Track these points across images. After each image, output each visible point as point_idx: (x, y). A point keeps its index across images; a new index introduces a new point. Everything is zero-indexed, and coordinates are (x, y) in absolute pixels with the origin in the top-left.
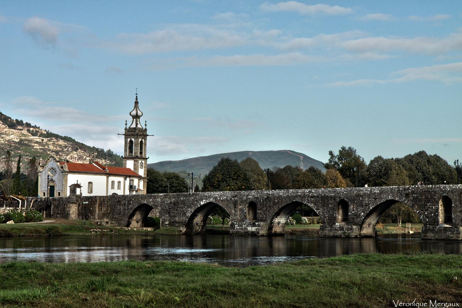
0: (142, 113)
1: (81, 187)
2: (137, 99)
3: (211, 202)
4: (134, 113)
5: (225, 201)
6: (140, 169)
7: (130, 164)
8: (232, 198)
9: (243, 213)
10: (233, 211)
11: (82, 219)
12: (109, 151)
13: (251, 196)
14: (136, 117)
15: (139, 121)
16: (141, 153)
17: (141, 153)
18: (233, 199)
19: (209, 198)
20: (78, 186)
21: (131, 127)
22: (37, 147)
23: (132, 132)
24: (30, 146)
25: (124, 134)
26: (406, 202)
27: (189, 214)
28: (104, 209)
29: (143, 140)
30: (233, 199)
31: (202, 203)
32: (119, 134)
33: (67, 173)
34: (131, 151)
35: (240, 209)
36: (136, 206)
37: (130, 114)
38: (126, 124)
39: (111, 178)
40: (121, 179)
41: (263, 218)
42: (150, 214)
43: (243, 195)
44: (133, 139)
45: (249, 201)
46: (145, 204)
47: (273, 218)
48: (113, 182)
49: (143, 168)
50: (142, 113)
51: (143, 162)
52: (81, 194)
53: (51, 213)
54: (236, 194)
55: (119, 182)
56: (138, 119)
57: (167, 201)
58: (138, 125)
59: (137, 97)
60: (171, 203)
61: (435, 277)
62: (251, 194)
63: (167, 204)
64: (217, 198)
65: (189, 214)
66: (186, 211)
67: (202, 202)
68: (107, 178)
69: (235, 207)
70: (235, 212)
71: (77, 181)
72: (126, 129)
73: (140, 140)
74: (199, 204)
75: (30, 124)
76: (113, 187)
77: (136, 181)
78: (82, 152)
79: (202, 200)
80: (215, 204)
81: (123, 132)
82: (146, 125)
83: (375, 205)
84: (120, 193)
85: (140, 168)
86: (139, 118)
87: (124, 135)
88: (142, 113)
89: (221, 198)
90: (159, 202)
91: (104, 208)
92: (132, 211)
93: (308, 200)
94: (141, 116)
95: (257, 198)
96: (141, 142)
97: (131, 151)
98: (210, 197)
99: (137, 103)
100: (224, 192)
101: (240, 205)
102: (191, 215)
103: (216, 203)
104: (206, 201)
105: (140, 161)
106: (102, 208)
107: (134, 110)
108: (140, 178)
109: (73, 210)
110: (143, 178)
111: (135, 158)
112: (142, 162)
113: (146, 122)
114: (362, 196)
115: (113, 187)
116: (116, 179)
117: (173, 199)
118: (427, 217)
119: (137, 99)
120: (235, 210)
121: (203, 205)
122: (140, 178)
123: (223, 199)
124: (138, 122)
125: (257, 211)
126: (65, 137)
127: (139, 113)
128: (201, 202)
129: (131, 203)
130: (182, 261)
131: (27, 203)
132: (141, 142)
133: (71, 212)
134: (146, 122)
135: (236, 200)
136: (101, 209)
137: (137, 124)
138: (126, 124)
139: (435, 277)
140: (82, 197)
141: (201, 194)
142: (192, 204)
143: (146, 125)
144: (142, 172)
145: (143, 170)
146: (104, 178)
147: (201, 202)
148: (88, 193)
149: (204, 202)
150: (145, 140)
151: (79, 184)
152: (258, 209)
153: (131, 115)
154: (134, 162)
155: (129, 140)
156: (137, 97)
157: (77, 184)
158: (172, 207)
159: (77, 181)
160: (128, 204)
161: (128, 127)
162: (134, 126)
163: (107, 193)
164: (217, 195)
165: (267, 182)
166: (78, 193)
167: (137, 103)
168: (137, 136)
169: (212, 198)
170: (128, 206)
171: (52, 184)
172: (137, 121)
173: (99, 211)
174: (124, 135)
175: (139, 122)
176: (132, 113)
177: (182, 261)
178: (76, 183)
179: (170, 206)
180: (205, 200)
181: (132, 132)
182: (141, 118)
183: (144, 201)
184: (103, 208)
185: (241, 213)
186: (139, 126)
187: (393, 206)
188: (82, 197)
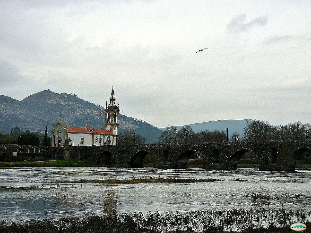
0: (116, 98)
2: (113, 89)
3: (242, 150)
7: (108, 128)
10: (155, 156)
11: (72, 160)
12: (140, 120)
16: (115, 121)
17: (115, 121)
22: (97, 117)
24: (93, 117)
27: (130, 158)
29: (116, 113)
35: (159, 155)
36: (102, 152)
37: (109, 98)
38: (107, 104)
39: (95, 136)
41: (172, 159)
44: (110, 113)
46: (107, 151)
47: (178, 160)
48: (97, 139)
51: (116, 126)
53: (56, 156)
59: (113, 88)
60: (121, 151)
69: (156, 153)
73: (114, 113)
76: (96, 141)
77: (111, 138)
82: (118, 105)
83: (234, 153)
93: (197, 149)
95: (169, 148)
108: (114, 136)
109: (67, 154)
111: (112, 124)
113: (107, 102)
114: (227, 147)
115: (96, 141)
118: (263, 160)
119: (113, 89)
122: (114, 136)
131: (43, 150)
132: (115, 114)
133: (66, 155)
134: (107, 102)
138: (107, 104)
143: (118, 105)
144: (115, 133)
156: (113, 88)
157: (70, 139)
162: (111, 105)
164: (147, 146)
166: (70, 144)
167: (113, 92)
170: (97, 152)
171: (59, 139)
172: (113, 102)
173: (81, 155)
175: (114, 103)
186: (114, 105)
187: (244, 155)
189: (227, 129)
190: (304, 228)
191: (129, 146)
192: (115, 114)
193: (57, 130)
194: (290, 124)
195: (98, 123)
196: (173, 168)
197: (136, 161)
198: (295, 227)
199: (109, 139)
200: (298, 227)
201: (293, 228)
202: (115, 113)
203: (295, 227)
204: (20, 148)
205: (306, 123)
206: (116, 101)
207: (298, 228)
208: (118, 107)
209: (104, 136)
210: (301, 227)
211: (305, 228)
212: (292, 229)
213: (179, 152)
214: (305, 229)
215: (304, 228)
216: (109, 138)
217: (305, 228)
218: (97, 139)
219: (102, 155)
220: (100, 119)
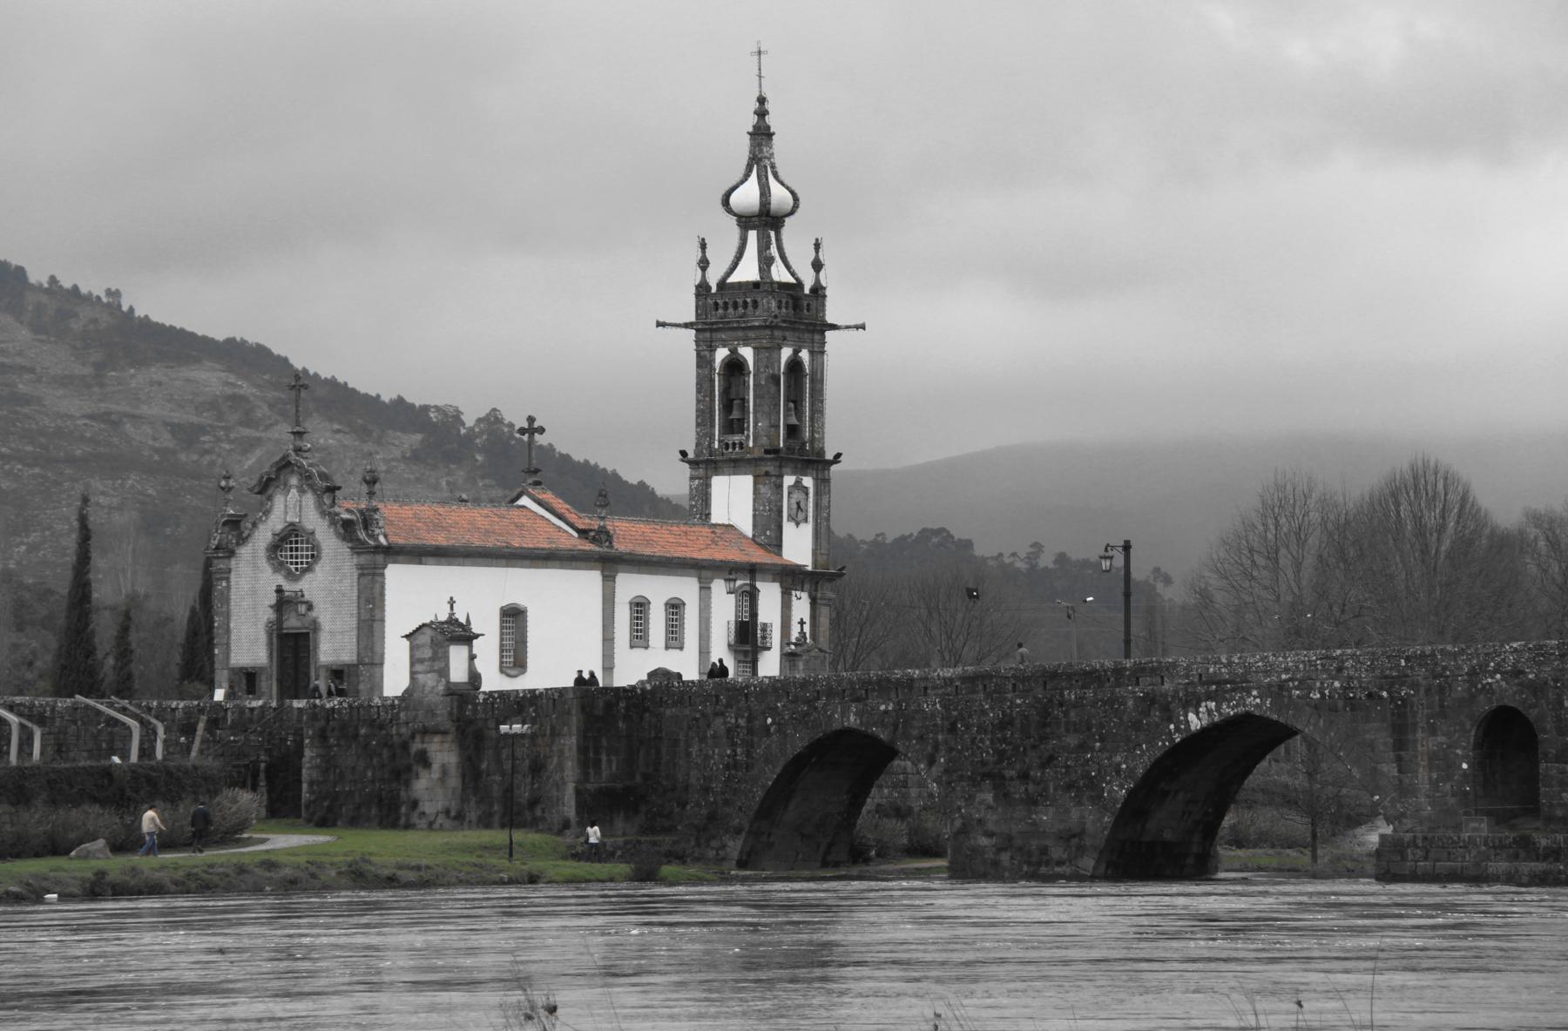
0: (796, 198)
1: (477, 636)
2: (762, 113)
3: (1248, 716)
4: (747, 196)
5: (1333, 709)
6: (788, 528)
8: (1382, 689)
9: (1448, 778)
10: (1390, 769)
13: (1498, 676)
14: (766, 221)
15: (779, 240)
18: (1385, 694)
19: (1233, 690)
20: (462, 634)
21: (732, 279)
23: (735, 306)
26: (1090, 572)
27: (1119, 791)
28: (609, 767)
29: (804, 355)
30: (1385, 694)
31: (1195, 722)
32: (857, 327)
33: (380, 558)
34: (734, 426)
35: (1432, 757)
36: (799, 741)
37: (726, 202)
38: (704, 264)
39: (629, 585)
40: (685, 588)
43: (1445, 668)
44: (747, 353)
45: (1484, 706)
48: (640, 607)
49: (806, 520)
50: (792, 193)
51: (808, 482)
52: (475, 678)
54: (1403, 663)
55: (638, 604)
56: (772, 234)
57: (984, 713)
58: (773, 268)
60: (1005, 723)
62: (1498, 664)
63: (986, 732)
64: (1289, 690)
65: (1121, 787)
66: (1099, 771)
67: (1197, 714)
68: (609, 579)
69: (1400, 744)
70: (1400, 771)
71: (452, 602)
72: (702, 289)
73: (786, 353)
74: (1177, 729)
75: (698, 287)
76: (639, 637)
78: (336, 427)
79: (1193, 702)
80: (1276, 722)
81: (687, 310)
82: (817, 266)
84: (688, 667)
85: (791, 518)
86: (778, 230)
87: (834, 327)
88: (796, 198)
89: (1311, 689)
90: (933, 715)
91: (613, 758)
92: (778, 770)
94: (792, 213)
95: (1537, 688)
96: (795, 365)
97: (734, 426)
98: (1240, 684)
99: (762, 134)
100: (1327, 657)
101: (1433, 731)
102: (1131, 793)
103: (1282, 720)
104: (1218, 708)
105: (789, 480)
106: (600, 761)
112: (734, 351)
113: (703, 246)
115: (639, 637)
116: (658, 589)
117: (1018, 701)
119: (762, 113)
120: (1399, 759)
121: (1203, 731)
122: (791, 578)
123: (1323, 694)
124: (774, 251)
125: (1543, 766)
126: (230, 342)
128: (1192, 717)
129: (767, 728)
135: (1402, 699)
136: (598, 763)
137: (765, 262)
138: (704, 264)
140: (481, 697)
141: (1188, 668)
142: (1137, 726)
143: (817, 266)
144: (798, 546)
145: (807, 530)
146: (591, 580)
147: (1192, 717)
148: (502, 670)
149: (1209, 712)
150: (818, 352)
151: (463, 620)
152: (1546, 754)
153: (729, 210)
154: (755, 483)
155: (722, 354)
157: (452, 621)
158: (1016, 748)
159: (452, 602)
160: (750, 731)
161: (713, 279)
162: (748, 271)
163: (608, 668)
164: (1287, 670)
165: (1228, 557)
167: (762, 134)
168: (768, 338)
169: (1255, 693)
171: (292, 623)
172: (763, 247)
176: (734, 199)
178: (443, 617)
179: (1004, 740)
180: (1212, 705)
181: (735, 306)
182: (790, 227)
183: (844, 714)
184: (604, 758)
185: (1437, 781)
186: (779, 274)
188: (481, 697)
189: (1127, 547)
191: (898, 684)
192: (795, 365)
193: (263, 536)
195: (71, 460)
196: (1537, 885)
197: (1165, 823)
199: (754, 614)
202: (796, 352)
206: (796, 239)
208: (818, 291)
209: (705, 589)
216: (750, 597)
218: (640, 607)
219: (797, 765)
220: (91, 417)
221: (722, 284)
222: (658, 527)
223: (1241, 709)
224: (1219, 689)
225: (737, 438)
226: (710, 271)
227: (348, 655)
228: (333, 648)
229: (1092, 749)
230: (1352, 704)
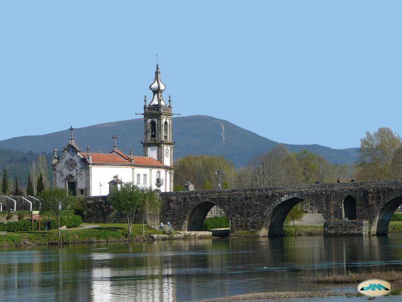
4: (155, 85)
6: (165, 158)
16: (153, 136)
25: (143, 113)
31: (283, 199)
37: (150, 88)
39: (138, 170)
40: (146, 171)
42: (209, 214)
44: (168, 121)
61: (158, 229)
68: (133, 169)
72: (145, 107)
77: (163, 171)
82: (170, 101)
87: (143, 114)
105: (165, 148)
107: (154, 82)
108: (166, 168)
110: (170, 169)
113: (145, 97)
121: (285, 201)
127: (162, 87)
130: (106, 256)
137: (159, 101)
139: (158, 229)
143: (170, 101)
149: (287, 197)
155: (149, 121)
162: (156, 102)
164: (303, 188)
167: (157, 73)
174: (143, 114)
176: (152, 87)
177: (106, 256)
190: (387, 289)
194: (111, 295)
198: (368, 288)
200: (373, 287)
201: (362, 289)
203: (368, 288)
204: (30, 204)
205: (374, 130)
206: (165, 95)
207: (375, 290)
210: (380, 287)
211: (388, 290)
212: (362, 292)
213: (77, 160)
214: (387, 292)
215: (387, 289)
217: (388, 290)
221: (149, 105)
222: (45, 164)
223: (293, 197)
224: (289, 194)
225: (154, 139)
226: (147, 102)
227: (84, 187)
228: (80, 185)
229: (88, 212)
230: (317, 195)
